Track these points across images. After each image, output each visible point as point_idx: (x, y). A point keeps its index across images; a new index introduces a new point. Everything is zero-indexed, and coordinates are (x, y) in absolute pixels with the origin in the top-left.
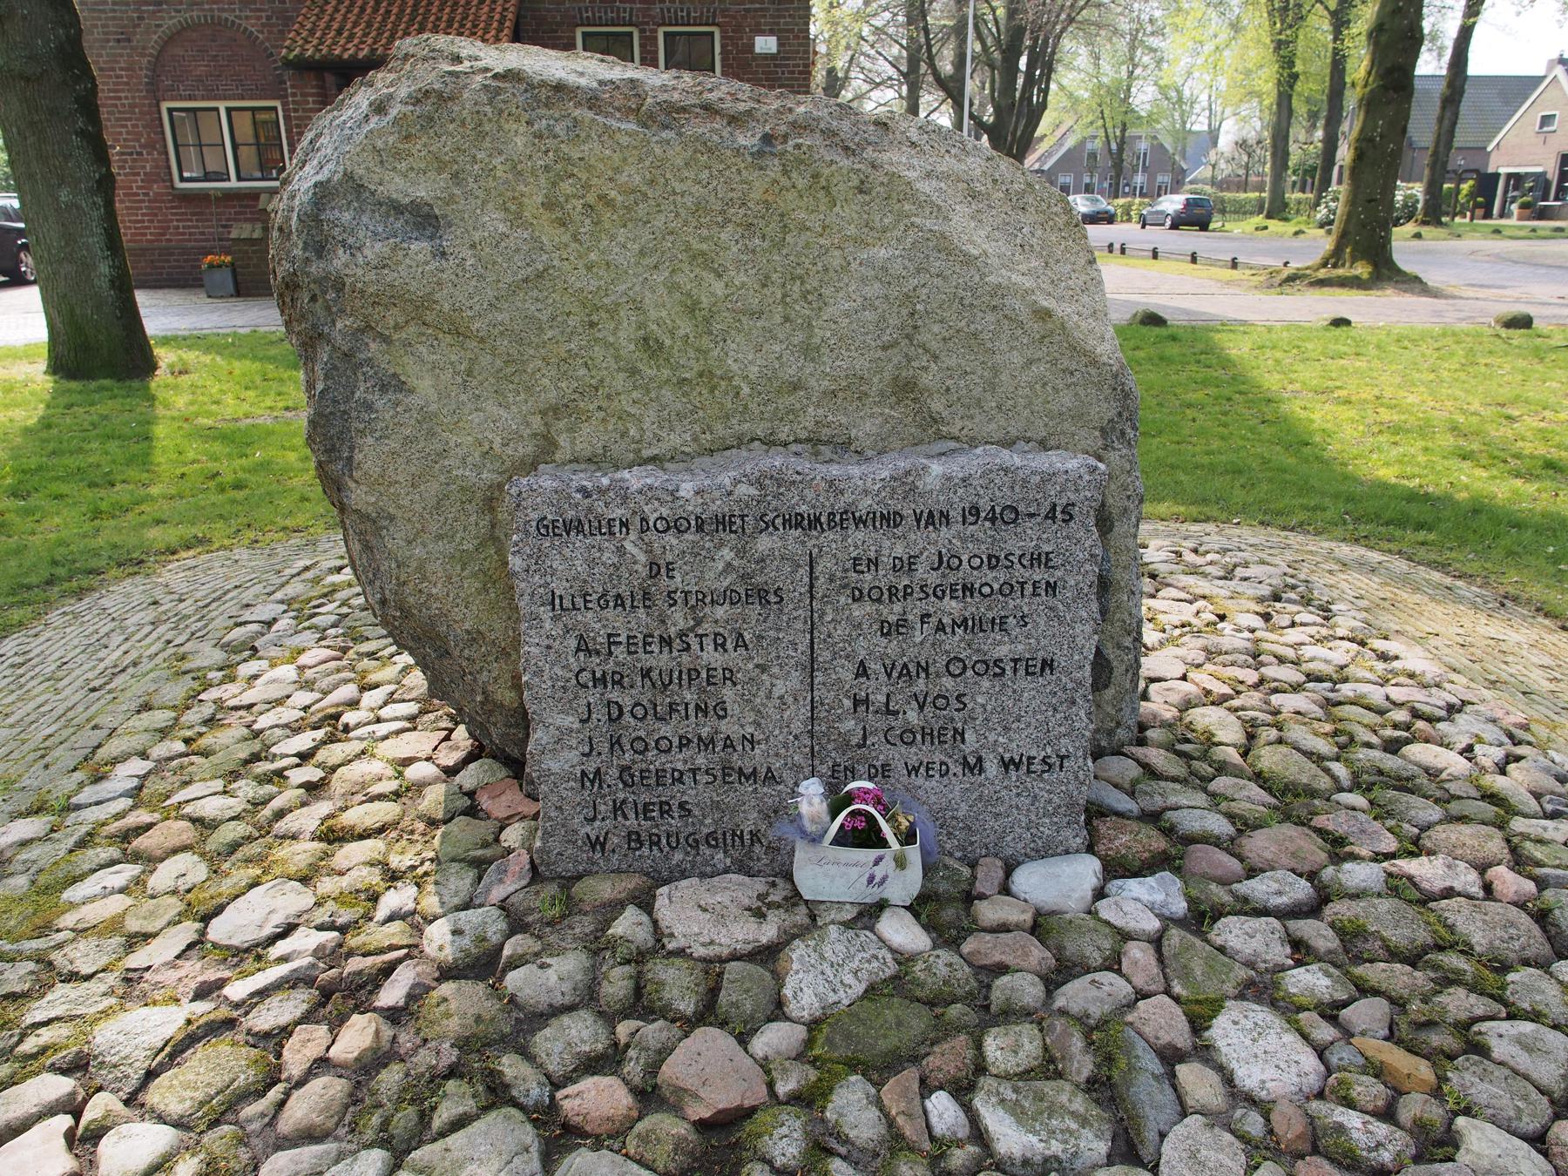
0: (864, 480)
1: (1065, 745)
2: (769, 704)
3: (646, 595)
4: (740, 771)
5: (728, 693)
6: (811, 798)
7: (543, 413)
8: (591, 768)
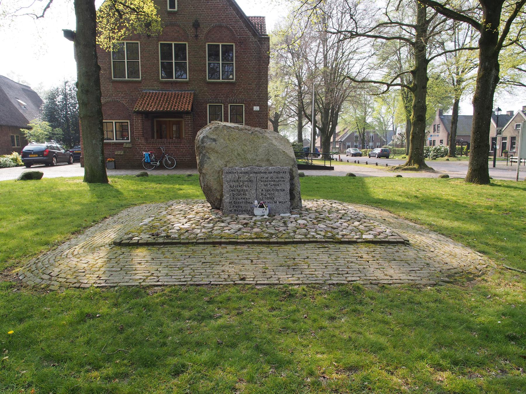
0: (263, 169)
1: (286, 200)
2: (251, 194)
5: (247, 193)
6: (256, 202)
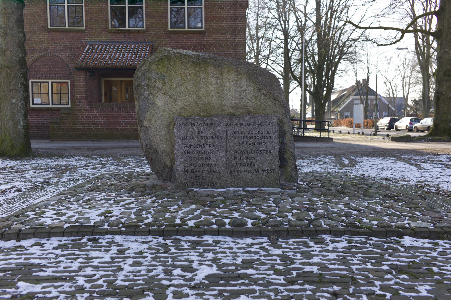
1: (274, 167)
3: (197, 137)
4: (214, 171)
5: (211, 155)
7: (180, 109)
8: (186, 169)
